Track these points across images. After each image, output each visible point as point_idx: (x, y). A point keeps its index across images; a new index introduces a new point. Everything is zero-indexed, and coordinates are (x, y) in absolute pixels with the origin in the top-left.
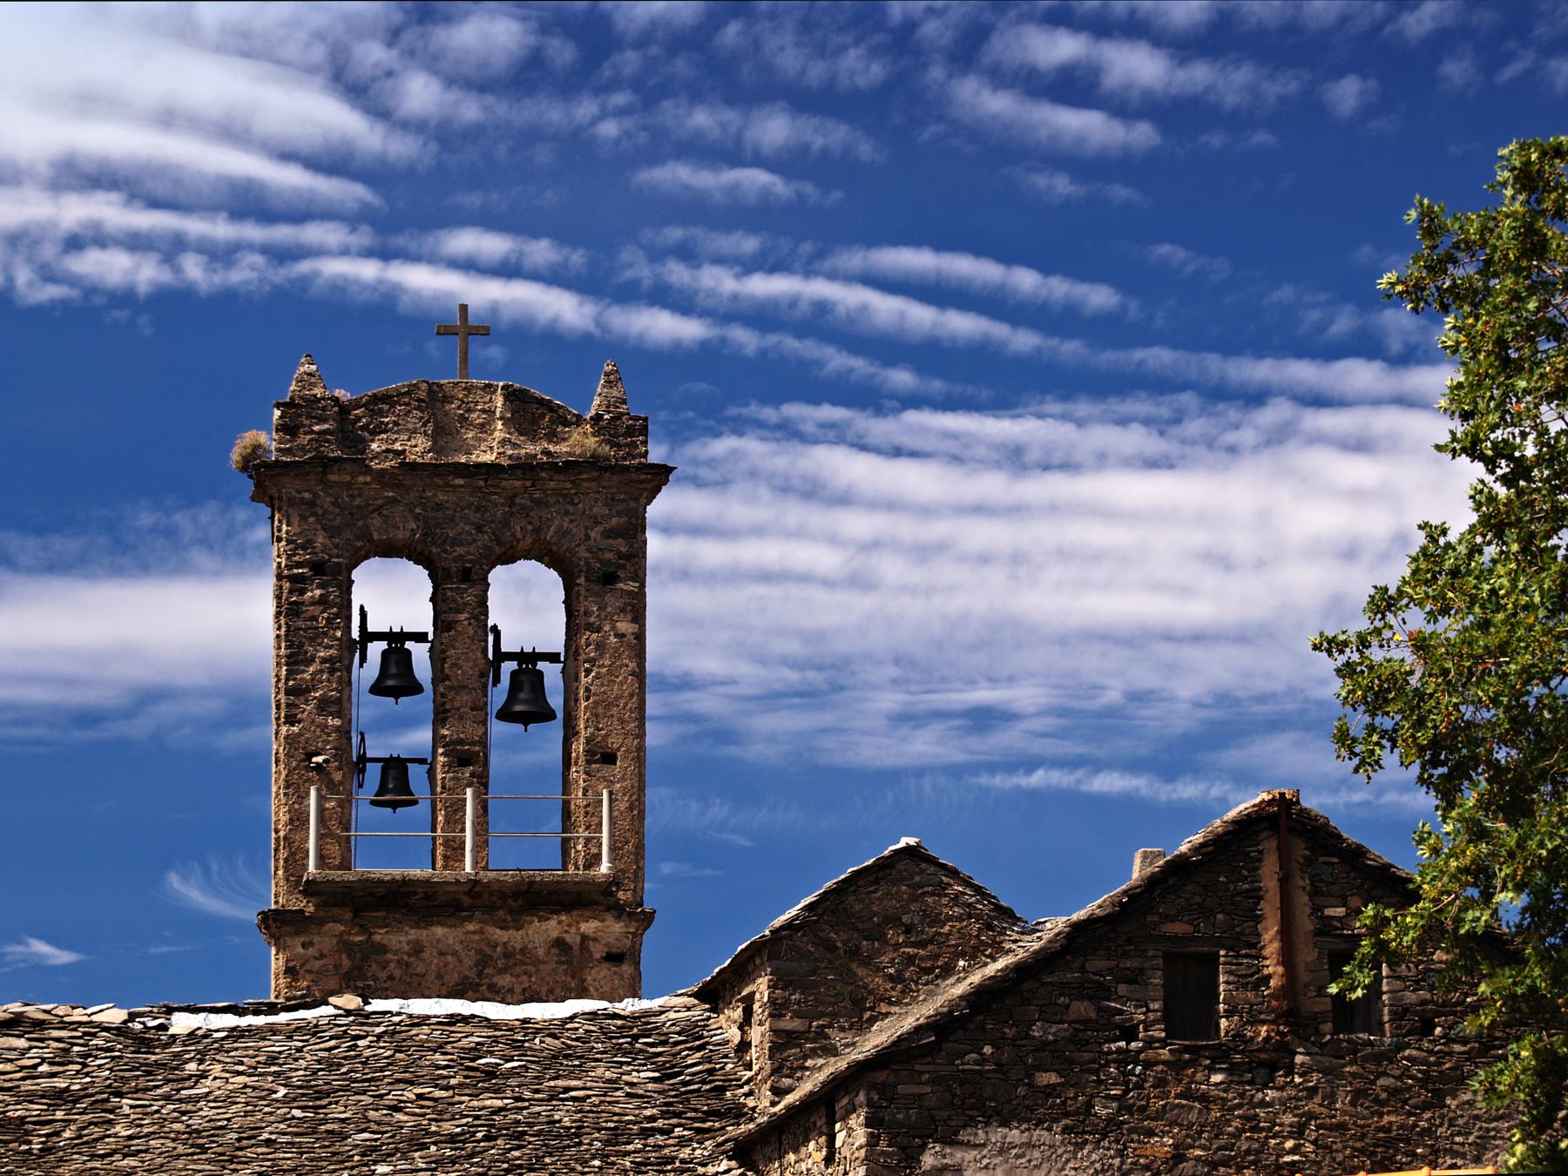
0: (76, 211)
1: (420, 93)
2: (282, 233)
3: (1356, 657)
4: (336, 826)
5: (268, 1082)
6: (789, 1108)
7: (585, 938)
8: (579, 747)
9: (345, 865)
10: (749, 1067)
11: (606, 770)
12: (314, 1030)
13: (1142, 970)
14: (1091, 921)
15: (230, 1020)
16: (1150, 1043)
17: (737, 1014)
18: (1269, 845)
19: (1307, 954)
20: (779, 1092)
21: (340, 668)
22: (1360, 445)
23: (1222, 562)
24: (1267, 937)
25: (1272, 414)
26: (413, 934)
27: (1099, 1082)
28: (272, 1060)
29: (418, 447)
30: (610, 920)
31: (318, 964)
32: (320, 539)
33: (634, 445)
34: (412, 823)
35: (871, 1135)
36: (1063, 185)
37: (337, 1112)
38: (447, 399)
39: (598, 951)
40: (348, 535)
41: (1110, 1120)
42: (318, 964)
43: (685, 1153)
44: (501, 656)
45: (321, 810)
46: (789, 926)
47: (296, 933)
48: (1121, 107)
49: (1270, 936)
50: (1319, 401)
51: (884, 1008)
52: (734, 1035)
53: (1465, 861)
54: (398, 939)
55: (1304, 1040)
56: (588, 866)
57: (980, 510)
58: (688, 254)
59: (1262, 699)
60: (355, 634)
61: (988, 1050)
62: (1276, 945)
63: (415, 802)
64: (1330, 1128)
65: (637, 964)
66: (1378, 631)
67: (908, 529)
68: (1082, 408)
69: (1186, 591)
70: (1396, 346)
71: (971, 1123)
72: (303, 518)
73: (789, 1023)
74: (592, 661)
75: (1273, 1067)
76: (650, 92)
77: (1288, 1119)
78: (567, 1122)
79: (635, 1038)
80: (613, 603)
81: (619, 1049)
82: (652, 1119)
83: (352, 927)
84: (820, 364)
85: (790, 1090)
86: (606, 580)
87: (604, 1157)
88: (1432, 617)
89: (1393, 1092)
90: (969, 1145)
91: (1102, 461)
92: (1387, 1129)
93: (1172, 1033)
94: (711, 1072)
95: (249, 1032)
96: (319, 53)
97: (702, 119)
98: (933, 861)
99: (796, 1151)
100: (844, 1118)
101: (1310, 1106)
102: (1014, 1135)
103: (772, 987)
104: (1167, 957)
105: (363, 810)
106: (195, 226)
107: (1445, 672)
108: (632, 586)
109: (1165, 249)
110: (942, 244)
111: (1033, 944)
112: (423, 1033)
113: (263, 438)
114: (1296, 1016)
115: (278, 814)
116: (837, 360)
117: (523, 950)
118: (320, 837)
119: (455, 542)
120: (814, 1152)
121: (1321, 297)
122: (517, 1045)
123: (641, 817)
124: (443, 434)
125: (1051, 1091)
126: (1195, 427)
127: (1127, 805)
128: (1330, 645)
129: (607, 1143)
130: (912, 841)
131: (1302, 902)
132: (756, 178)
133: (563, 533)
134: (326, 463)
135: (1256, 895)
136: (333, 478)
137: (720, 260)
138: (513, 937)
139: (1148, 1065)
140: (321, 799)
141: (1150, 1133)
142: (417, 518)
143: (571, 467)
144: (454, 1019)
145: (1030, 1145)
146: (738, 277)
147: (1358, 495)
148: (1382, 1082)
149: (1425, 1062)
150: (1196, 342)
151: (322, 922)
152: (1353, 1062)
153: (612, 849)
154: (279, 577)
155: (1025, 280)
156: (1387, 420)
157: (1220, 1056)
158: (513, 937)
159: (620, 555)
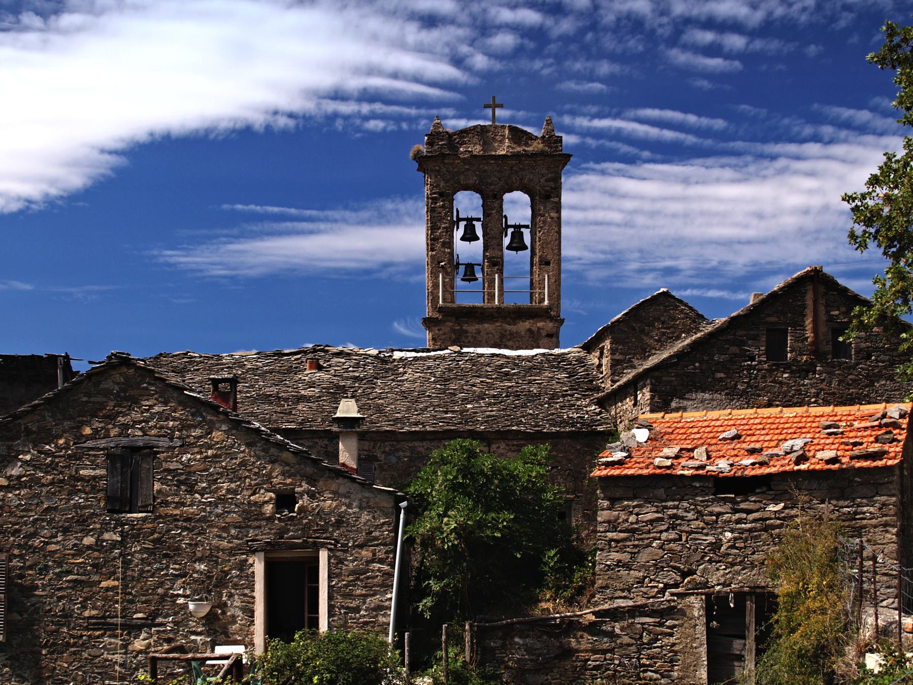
0: (365, 108)
1: (480, 61)
2: (434, 112)
3: (859, 204)
4: (449, 288)
5: (428, 376)
6: (619, 386)
7: (539, 328)
8: (536, 259)
9: (453, 302)
10: (602, 373)
11: (547, 268)
12: (443, 358)
13: (758, 335)
14: (738, 316)
15: (414, 354)
16: (760, 362)
17: (598, 354)
18: (810, 288)
19: (823, 329)
20: (614, 382)
21: (450, 232)
22: (811, 174)
23: (760, 216)
24: (807, 322)
25: (781, 163)
26: (477, 326)
27: (740, 377)
28: (429, 368)
29: (477, 149)
30: (548, 321)
31: (443, 337)
32: (442, 184)
33: (557, 147)
34: (477, 286)
35: (652, 396)
36: (705, 84)
37: (452, 386)
38: (488, 131)
39: (544, 333)
40: (452, 182)
41: (744, 391)
42: (443, 337)
43: (579, 403)
44: (508, 226)
45: (443, 282)
46: (618, 321)
47: (436, 326)
48: (729, 56)
49: (808, 322)
50: (798, 158)
51: (653, 351)
52: (596, 361)
53: (899, 287)
54: (472, 328)
55: (820, 362)
56: (540, 303)
57: (673, 199)
58: (573, 113)
59: (770, 263)
60: (455, 219)
61: (697, 364)
62: (811, 326)
63: (477, 279)
64: (829, 394)
65: (558, 337)
66: (870, 193)
67: (647, 206)
68: (710, 161)
69: (746, 226)
70: (826, 139)
71: (690, 391)
72: (436, 176)
73: (618, 357)
74: (541, 228)
75: (808, 372)
76: (559, 58)
77: (813, 390)
78: (535, 391)
79: (559, 362)
80: (549, 206)
81: (553, 366)
82: (566, 391)
83: (454, 323)
84: (618, 150)
85: (618, 381)
86: (546, 199)
87: (549, 404)
88: (891, 189)
89: (854, 381)
90: (689, 399)
91: (718, 181)
92: (851, 394)
93: (768, 359)
94: (588, 375)
95: (421, 358)
96: (447, 50)
97: (578, 66)
98: (673, 297)
99: (622, 402)
100: (641, 389)
101: (822, 386)
102: (707, 396)
103: (611, 343)
104: (768, 330)
105: (459, 282)
106: (406, 110)
107: (901, 209)
108: (556, 199)
109: (743, 106)
110: (662, 108)
111: (710, 329)
112: (482, 360)
113: (421, 148)
114: (817, 353)
115: (428, 283)
116: (625, 148)
117: (517, 333)
118: (443, 292)
119: (491, 184)
120: (629, 402)
121: (799, 122)
122: (516, 365)
123: (559, 285)
124: (486, 144)
125: (721, 380)
126: (752, 168)
127: (720, 300)
128: (848, 198)
129: (550, 399)
130: (665, 290)
131: (822, 309)
132: (597, 86)
133: (531, 180)
134: (444, 156)
135: (804, 307)
136: (446, 161)
137: (584, 115)
138: (513, 328)
139: (759, 370)
140: (443, 278)
141: (759, 395)
142: (477, 175)
143: (534, 155)
144: (493, 355)
145: (712, 400)
146: (590, 120)
147: (810, 192)
148: (850, 377)
149: (868, 370)
150: (754, 139)
151: (445, 321)
152: (839, 370)
153: (549, 296)
154: (428, 198)
155: (692, 119)
156: (821, 165)
157: (787, 367)
158: (513, 328)
159: (552, 188)
